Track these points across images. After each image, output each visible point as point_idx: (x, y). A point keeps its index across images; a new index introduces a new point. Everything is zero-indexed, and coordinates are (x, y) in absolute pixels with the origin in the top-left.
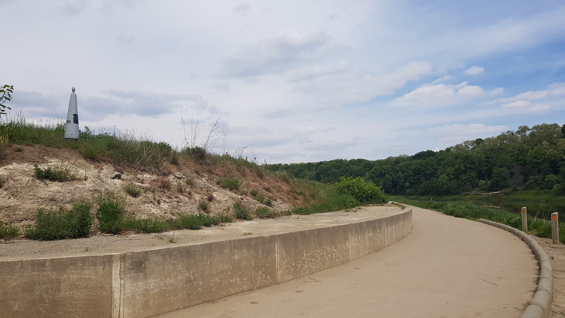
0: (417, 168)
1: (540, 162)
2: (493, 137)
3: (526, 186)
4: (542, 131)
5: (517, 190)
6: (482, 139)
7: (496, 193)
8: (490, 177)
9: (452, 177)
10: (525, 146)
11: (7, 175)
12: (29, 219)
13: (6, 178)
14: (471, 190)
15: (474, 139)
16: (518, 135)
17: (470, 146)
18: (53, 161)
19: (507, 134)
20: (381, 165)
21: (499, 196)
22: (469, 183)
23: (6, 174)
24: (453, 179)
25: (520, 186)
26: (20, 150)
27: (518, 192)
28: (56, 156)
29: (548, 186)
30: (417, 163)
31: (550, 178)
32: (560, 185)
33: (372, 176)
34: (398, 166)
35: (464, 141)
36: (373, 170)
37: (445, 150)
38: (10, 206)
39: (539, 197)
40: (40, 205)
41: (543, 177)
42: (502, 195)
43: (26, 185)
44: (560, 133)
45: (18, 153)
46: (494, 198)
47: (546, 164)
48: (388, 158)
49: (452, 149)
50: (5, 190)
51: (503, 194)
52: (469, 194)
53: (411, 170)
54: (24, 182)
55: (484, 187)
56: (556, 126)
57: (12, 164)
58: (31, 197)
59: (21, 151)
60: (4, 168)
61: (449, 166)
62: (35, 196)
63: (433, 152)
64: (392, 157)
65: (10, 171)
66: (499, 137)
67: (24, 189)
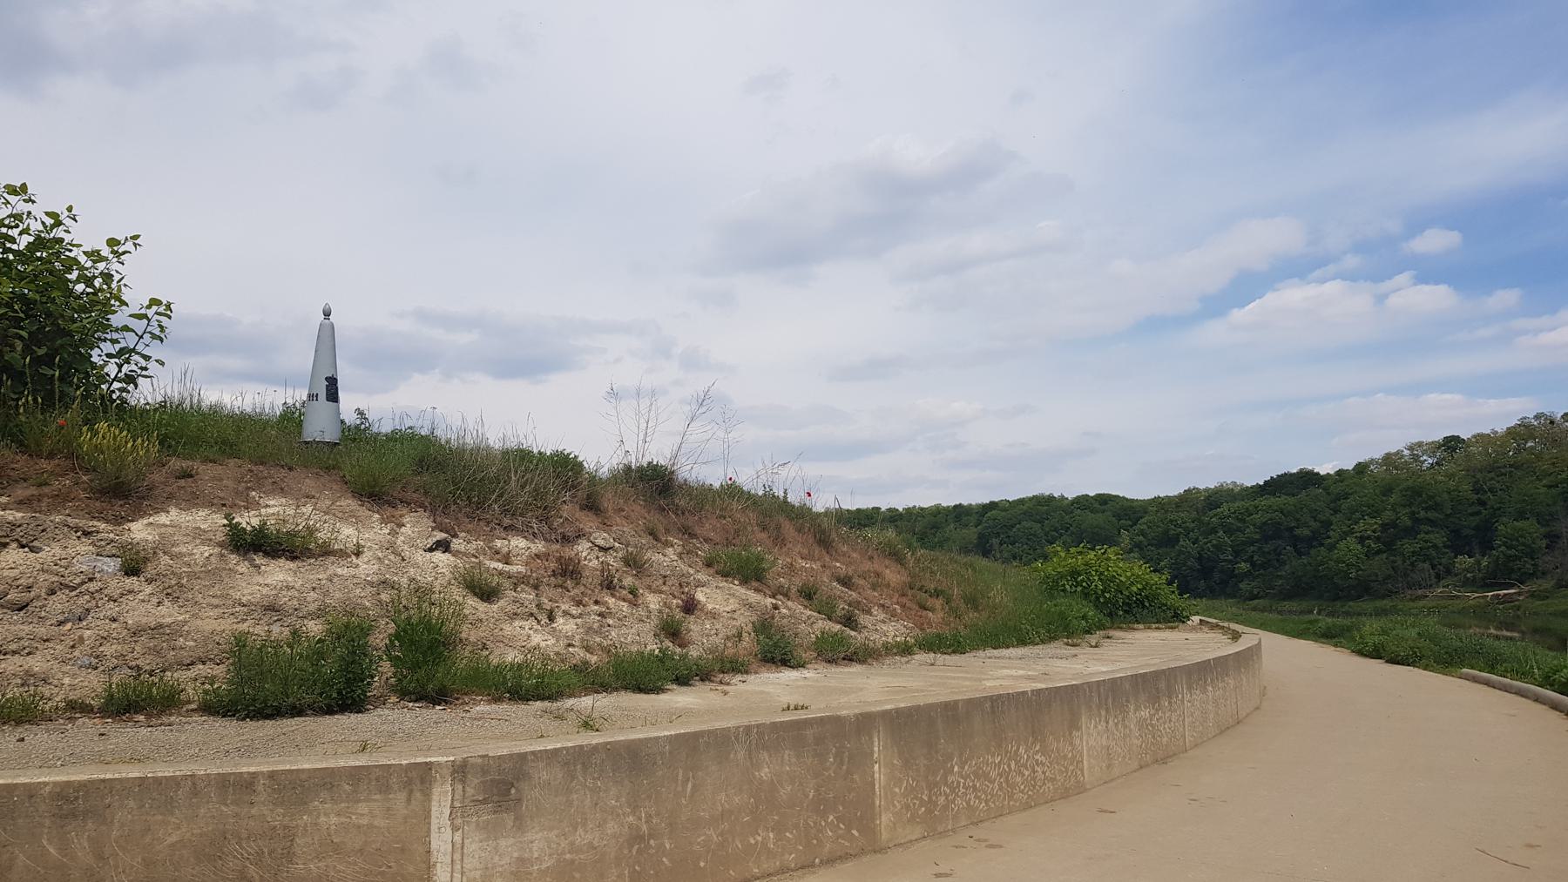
0: (1271, 519)
7: (1505, 595)
8: (1487, 546)
11: (154, 542)
12: (210, 660)
13: (152, 548)
15: (1439, 436)
18: (272, 503)
19: (1535, 423)
20: (1166, 512)
21: (1516, 603)
22: (1427, 565)
23: (150, 538)
24: (1379, 552)
26: (187, 475)
28: (282, 489)
30: (1270, 506)
33: (1141, 542)
34: (1215, 515)
37: (1353, 469)
38: (161, 626)
45: (182, 482)
46: (1501, 607)
50: (149, 581)
55: (1469, 575)
57: (168, 512)
58: (215, 601)
60: (145, 521)
61: (1363, 516)
62: (226, 596)
63: (1318, 474)
65: (163, 530)
66: (1511, 432)
67: (198, 578)
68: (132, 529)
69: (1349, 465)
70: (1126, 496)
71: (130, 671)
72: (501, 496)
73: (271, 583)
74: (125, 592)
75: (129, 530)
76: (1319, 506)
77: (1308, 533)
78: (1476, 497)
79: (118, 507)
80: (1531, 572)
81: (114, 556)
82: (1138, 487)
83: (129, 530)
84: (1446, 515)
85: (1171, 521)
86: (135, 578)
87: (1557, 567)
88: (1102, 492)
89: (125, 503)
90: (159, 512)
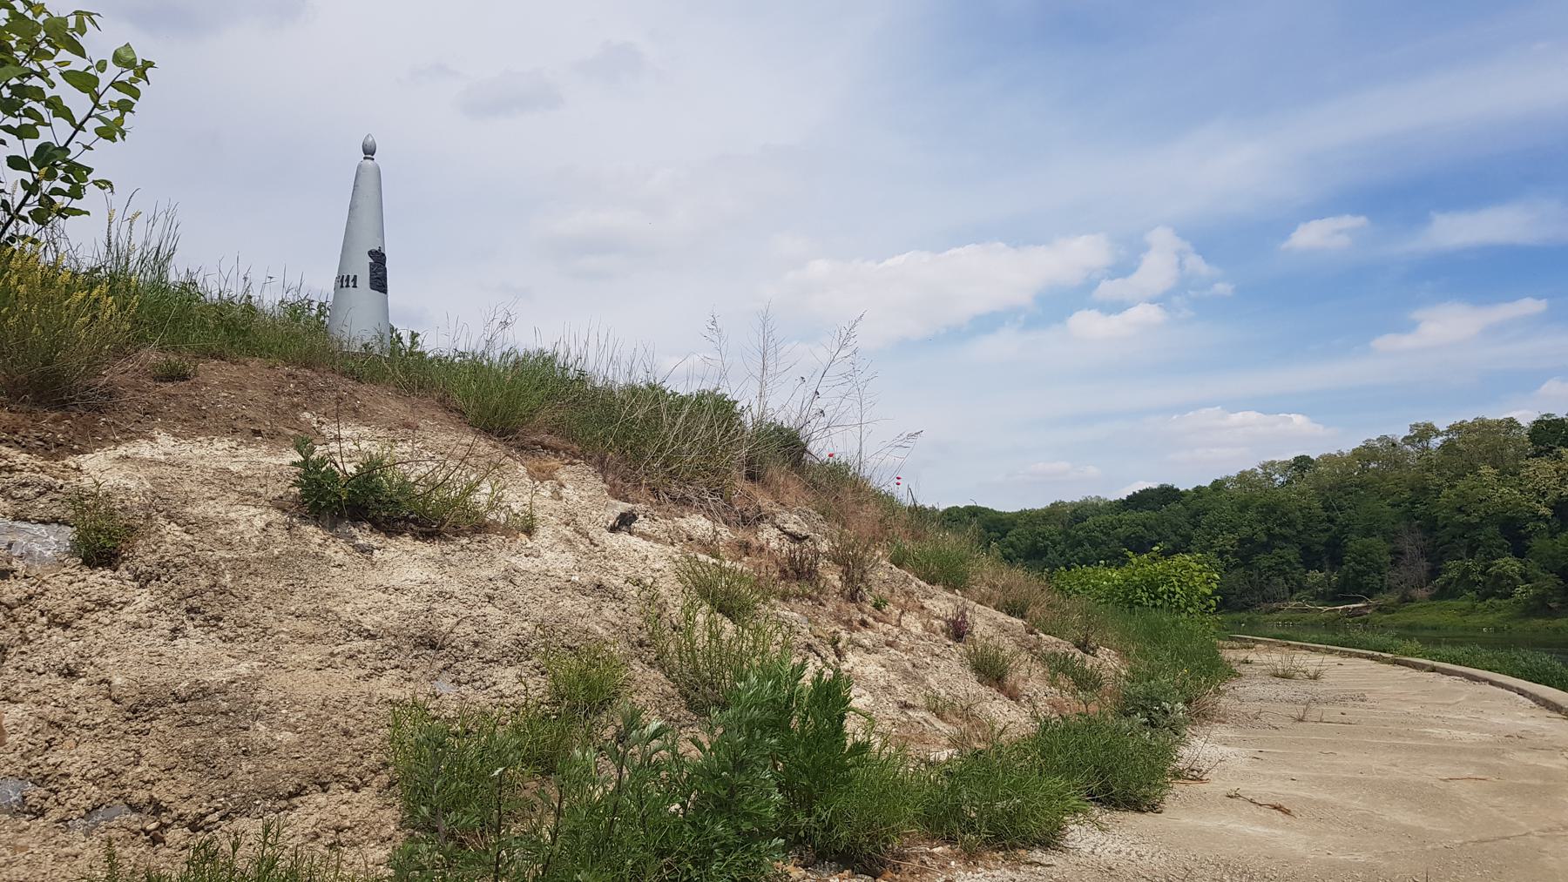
0: (1133, 533)
1: (1473, 522)
2: (1341, 453)
3: (1436, 589)
4: (1475, 436)
5: (1412, 600)
6: (1311, 457)
7: (1354, 608)
8: (1336, 562)
9: (1231, 560)
10: (1433, 478)
11: (144, 493)
12: (340, 778)
13: (146, 507)
14: (1285, 599)
15: (1290, 457)
16: (1409, 447)
17: (1277, 476)
19: (1378, 445)
20: (1035, 524)
21: (1365, 616)
22: (1281, 580)
23: (132, 485)
24: (1236, 566)
25: (1421, 587)
27: (1414, 605)
28: (355, 410)
29: (1497, 588)
31: (1503, 566)
32: (1532, 588)
33: (1010, 554)
34: (1081, 529)
35: (1262, 463)
36: (1011, 537)
37: (1211, 486)
38: (204, 692)
39: (1473, 620)
40: (370, 676)
41: (1485, 563)
42: (1371, 614)
43: (261, 553)
44: (1524, 442)
45: (168, 387)
46: (1350, 620)
47: (1492, 530)
48: (1052, 504)
49: (1228, 484)
51: (1374, 609)
52: (1280, 609)
53: (1119, 539)
54: (247, 537)
55: (1320, 589)
56: (1511, 423)
57: (152, 439)
58: (307, 627)
59: (184, 378)
61: (1222, 531)
62: (321, 615)
63: (1178, 490)
64: (1063, 502)
65: (154, 471)
66: (1356, 453)
67: (255, 573)
68: (84, 467)
69: (1206, 483)
70: (995, 509)
71: (135, 817)
72: (660, 450)
73: (408, 584)
74: (90, 606)
75: (78, 469)
76: (1180, 521)
77: (1170, 547)
78: (1326, 514)
79: (49, 423)
80: (1379, 587)
81: (55, 520)
82: (1006, 504)
83: (78, 469)
84: (1298, 532)
85: (1039, 533)
86: (108, 572)
87: (1402, 583)
88: (951, 506)
89: (63, 418)
90: (132, 438)
